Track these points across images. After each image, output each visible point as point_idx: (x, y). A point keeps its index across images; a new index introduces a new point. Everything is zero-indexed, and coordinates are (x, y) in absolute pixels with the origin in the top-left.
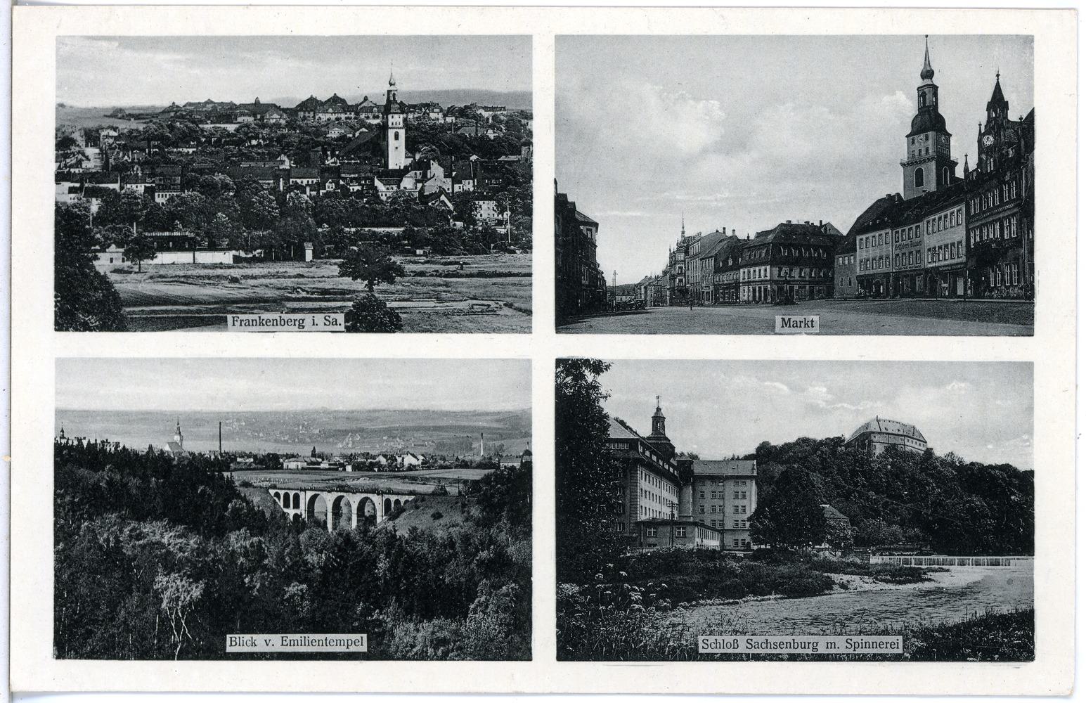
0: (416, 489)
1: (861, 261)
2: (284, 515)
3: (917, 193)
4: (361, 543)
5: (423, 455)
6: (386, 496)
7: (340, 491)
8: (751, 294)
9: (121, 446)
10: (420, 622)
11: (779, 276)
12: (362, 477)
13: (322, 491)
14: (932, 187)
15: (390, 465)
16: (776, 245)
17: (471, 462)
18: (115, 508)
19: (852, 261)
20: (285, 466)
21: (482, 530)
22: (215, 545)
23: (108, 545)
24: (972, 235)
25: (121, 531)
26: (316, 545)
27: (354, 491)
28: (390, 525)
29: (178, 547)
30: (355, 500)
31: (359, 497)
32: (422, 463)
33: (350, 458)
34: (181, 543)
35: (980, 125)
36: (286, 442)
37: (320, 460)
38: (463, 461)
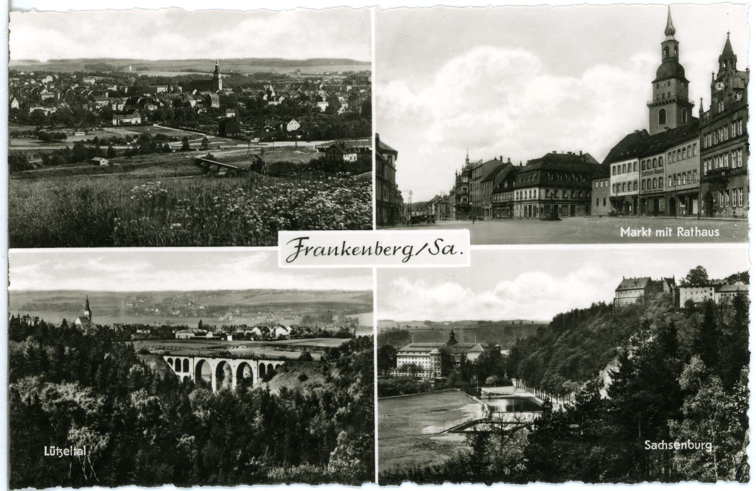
0: (286, 355)
1: (614, 185)
2: (177, 378)
3: (661, 130)
4: (240, 401)
5: (291, 327)
6: (260, 362)
7: (222, 357)
8: (523, 211)
9: (40, 320)
10: (289, 467)
11: (546, 197)
12: (241, 345)
13: (208, 357)
14: (674, 126)
15: (264, 335)
16: (543, 170)
17: (332, 332)
18: (35, 373)
19: (607, 185)
20: (177, 336)
21: (341, 390)
22: (118, 403)
23: (29, 403)
24: (705, 164)
25: (40, 391)
26: (203, 403)
27: (235, 357)
28: (264, 386)
29: (87, 405)
30: (234, 364)
31: (238, 362)
32: (291, 334)
33: (231, 329)
34: (90, 402)
35: (713, 74)
36: (177, 316)
37: (205, 331)
38: (325, 332)
